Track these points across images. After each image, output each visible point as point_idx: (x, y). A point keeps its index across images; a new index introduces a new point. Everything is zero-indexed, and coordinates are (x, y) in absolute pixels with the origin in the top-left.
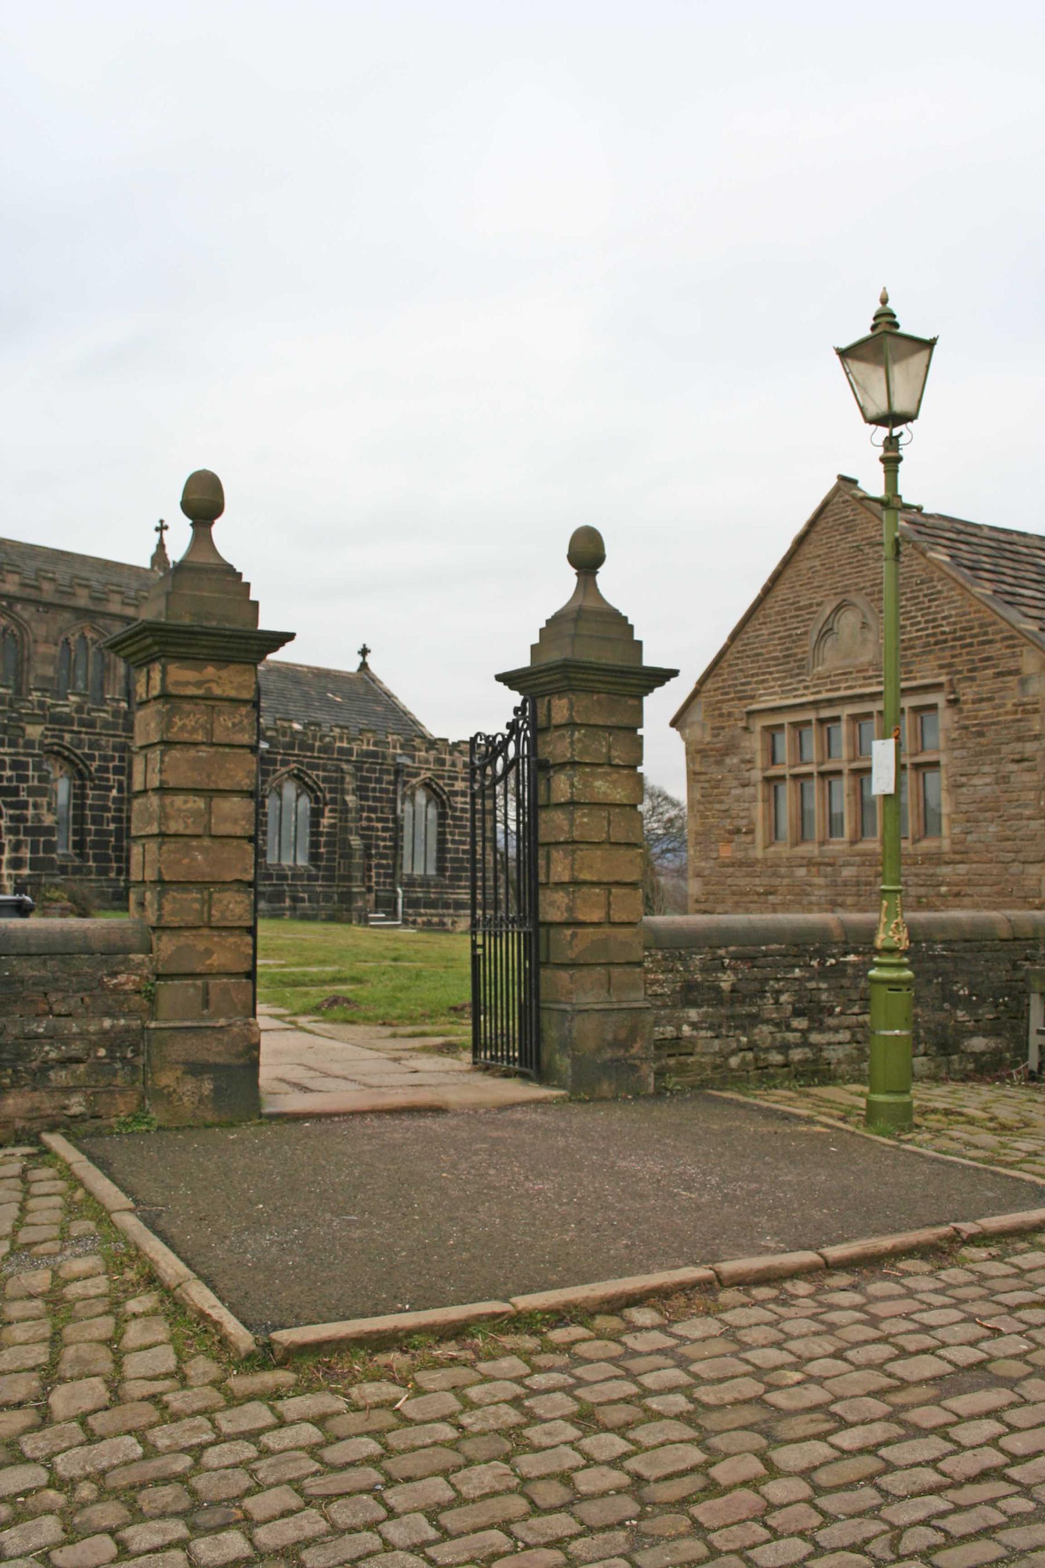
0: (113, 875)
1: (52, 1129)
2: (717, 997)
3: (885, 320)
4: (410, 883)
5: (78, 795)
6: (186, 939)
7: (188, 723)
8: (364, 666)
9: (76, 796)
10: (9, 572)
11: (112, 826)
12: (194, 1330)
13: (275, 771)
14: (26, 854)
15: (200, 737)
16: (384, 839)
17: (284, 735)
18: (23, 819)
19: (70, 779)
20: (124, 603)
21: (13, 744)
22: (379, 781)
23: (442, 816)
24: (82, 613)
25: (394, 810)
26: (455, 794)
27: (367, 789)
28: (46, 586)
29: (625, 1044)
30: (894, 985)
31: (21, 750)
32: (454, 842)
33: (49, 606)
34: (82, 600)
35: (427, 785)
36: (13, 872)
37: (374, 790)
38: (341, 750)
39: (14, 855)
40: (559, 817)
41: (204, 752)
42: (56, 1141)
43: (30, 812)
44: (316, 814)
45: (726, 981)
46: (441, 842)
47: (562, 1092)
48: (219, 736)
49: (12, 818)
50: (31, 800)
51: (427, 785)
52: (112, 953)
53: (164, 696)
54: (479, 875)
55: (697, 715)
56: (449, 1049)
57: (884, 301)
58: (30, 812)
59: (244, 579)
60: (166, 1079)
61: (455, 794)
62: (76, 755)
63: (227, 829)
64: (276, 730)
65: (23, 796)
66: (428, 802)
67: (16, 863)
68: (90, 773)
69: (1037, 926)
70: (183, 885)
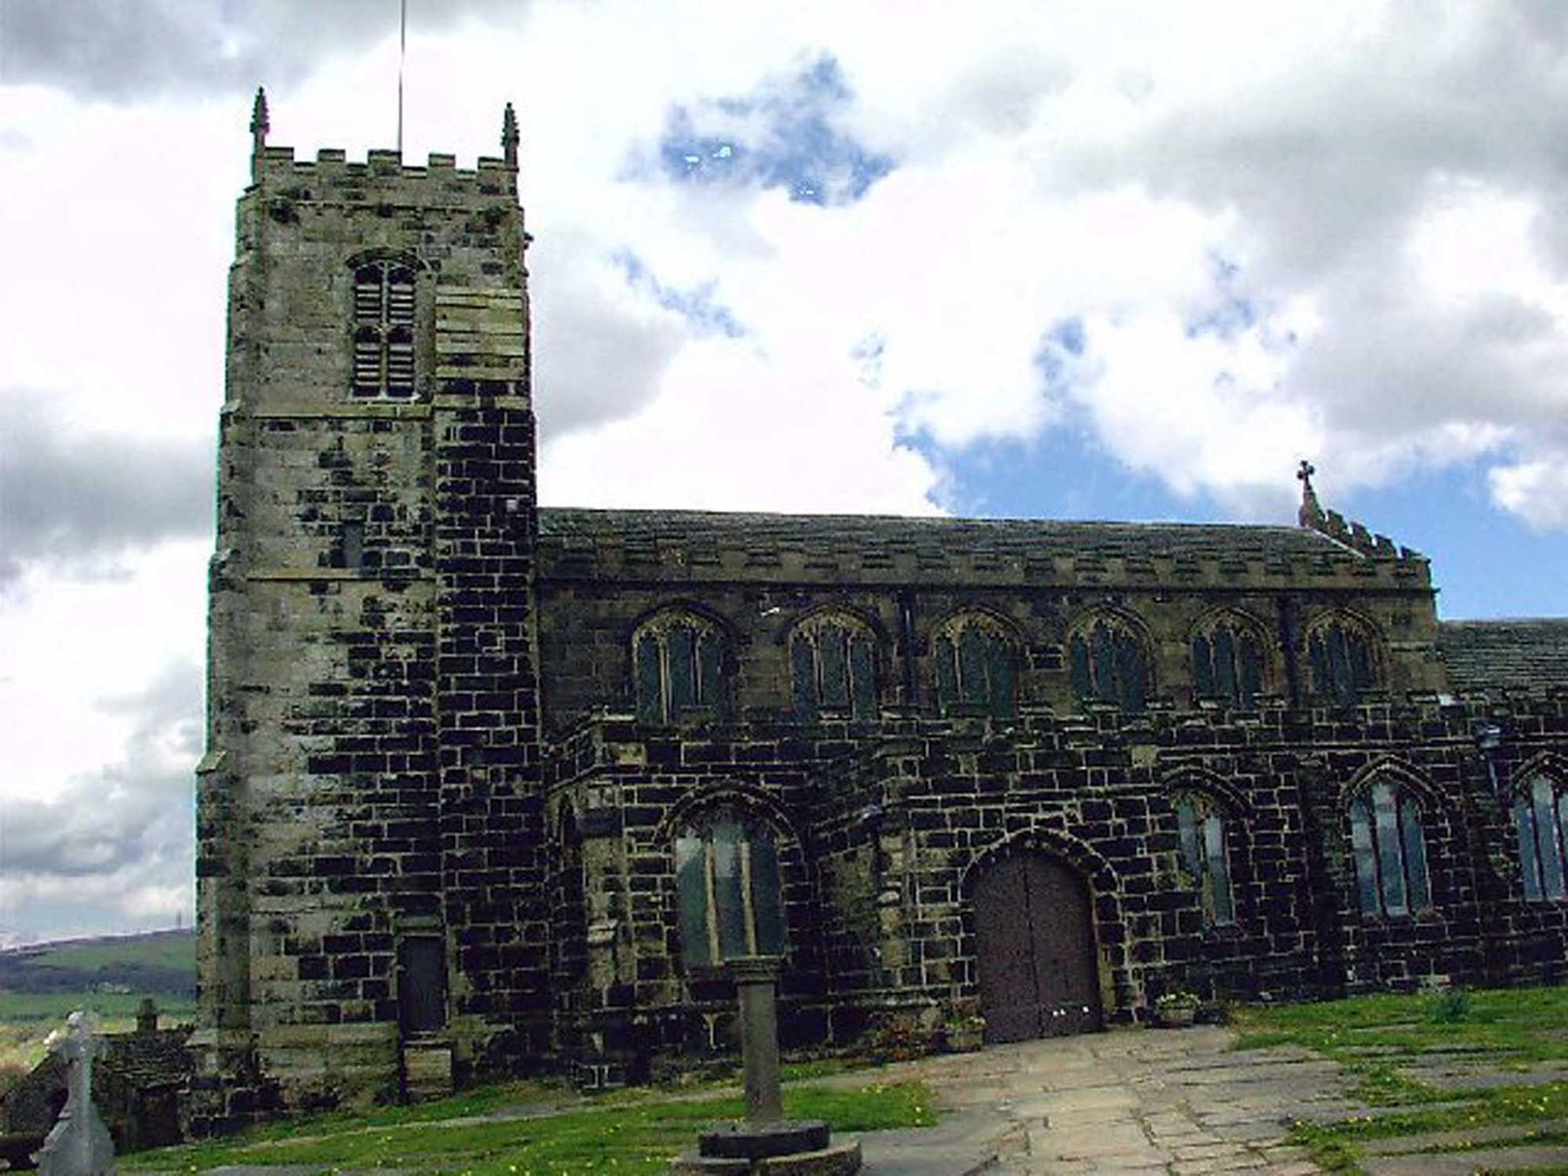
0: (1300, 947)
5: (1234, 839)
9: (1232, 842)
10: (1109, 556)
11: (1290, 878)
13: (1516, 766)
14: (1155, 936)
17: (1521, 711)
18: (1147, 885)
19: (1223, 818)
20: (1268, 572)
21: (1115, 777)
24: (1213, 595)
28: (1161, 567)
31: (1130, 786)
33: (1167, 593)
34: (1212, 576)
36: (1140, 965)
39: (1138, 940)
43: (1155, 875)
50: (1153, 856)
54: (1209, 782)
58: (1155, 875)
59: (415, 157)
62: (1224, 784)
64: (1508, 706)
67: (1144, 952)
68: (1246, 804)
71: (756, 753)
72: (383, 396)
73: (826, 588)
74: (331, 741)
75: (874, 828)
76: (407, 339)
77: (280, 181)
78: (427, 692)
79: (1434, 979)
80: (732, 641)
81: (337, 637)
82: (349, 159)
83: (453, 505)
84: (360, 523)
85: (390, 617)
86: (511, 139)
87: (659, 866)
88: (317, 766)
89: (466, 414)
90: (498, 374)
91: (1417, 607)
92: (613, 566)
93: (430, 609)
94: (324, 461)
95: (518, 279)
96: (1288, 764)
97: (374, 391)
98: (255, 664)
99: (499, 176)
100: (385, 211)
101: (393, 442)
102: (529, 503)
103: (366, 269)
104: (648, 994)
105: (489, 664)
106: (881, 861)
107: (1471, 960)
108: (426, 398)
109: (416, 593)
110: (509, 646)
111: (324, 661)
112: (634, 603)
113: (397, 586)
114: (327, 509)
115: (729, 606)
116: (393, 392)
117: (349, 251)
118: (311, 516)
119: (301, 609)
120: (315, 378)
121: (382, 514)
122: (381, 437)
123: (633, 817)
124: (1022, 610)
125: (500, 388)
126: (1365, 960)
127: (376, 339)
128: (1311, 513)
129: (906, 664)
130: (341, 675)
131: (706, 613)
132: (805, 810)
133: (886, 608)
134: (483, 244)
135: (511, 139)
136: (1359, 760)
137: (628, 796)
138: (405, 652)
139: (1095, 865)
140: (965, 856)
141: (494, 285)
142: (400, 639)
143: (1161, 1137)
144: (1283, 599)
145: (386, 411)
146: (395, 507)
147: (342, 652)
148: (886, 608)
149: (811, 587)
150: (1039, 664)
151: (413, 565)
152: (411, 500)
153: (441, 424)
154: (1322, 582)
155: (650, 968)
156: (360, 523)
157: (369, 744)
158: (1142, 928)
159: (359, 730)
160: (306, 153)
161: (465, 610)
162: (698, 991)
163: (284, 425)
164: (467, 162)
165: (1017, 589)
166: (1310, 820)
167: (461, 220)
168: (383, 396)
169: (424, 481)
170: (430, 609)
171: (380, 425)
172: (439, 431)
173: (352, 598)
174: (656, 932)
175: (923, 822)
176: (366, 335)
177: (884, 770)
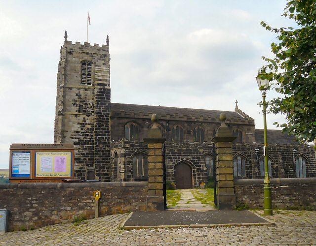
2: (251, 194)
6: (152, 184)
14: (201, 176)
16: (291, 169)
22: (288, 156)
23: (307, 163)
26: (310, 158)
27: (285, 158)
28: (209, 119)
29: (230, 201)
32: (310, 169)
35: (302, 156)
37: (287, 158)
38: (278, 149)
41: (154, 157)
44: (273, 164)
45: (253, 191)
46: (307, 169)
49: (198, 169)
52: (142, 186)
59: (92, 44)
61: (310, 158)
65: (200, 164)
66: (302, 160)
69: (315, 180)
74: (77, 140)
81: (79, 123)
85: (87, 121)
86: (108, 41)
87: (131, 162)
89: (100, 89)
90: (105, 83)
91: (251, 127)
94: (77, 95)
97: (85, 84)
99: (105, 48)
101: (88, 92)
103: (83, 63)
105: (103, 129)
108: (93, 86)
110: (106, 126)
111: (77, 127)
112: (125, 121)
113: (89, 116)
114: (77, 103)
115: (140, 122)
117: (81, 60)
118: (75, 104)
119: (73, 119)
120: (75, 80)
121: (86, 104)
130: (79, 130)
131: (134, 122)
134: (103, 60)
135: (108, 41)
136: (236, 153)
138: (89, 127)
139: (193, 165)
140: (174, 163)
141: (104, 67)
142: (89, 124)
145: (87, 88)
146: (88, 103)
147: (79, 126)
151: (91, 112)
152: (91, 102)
153: (96, 91)
154: (235, 123)
157: (83, 140)
158: (199, 175)
159: (82, 138)
161: (99, 121)
163: (71, 89)
164: (100, 45)
165: (185, 121)
169: (93, 99)
171: (86, 90)
174: (130, 171)
175: (169, 158)
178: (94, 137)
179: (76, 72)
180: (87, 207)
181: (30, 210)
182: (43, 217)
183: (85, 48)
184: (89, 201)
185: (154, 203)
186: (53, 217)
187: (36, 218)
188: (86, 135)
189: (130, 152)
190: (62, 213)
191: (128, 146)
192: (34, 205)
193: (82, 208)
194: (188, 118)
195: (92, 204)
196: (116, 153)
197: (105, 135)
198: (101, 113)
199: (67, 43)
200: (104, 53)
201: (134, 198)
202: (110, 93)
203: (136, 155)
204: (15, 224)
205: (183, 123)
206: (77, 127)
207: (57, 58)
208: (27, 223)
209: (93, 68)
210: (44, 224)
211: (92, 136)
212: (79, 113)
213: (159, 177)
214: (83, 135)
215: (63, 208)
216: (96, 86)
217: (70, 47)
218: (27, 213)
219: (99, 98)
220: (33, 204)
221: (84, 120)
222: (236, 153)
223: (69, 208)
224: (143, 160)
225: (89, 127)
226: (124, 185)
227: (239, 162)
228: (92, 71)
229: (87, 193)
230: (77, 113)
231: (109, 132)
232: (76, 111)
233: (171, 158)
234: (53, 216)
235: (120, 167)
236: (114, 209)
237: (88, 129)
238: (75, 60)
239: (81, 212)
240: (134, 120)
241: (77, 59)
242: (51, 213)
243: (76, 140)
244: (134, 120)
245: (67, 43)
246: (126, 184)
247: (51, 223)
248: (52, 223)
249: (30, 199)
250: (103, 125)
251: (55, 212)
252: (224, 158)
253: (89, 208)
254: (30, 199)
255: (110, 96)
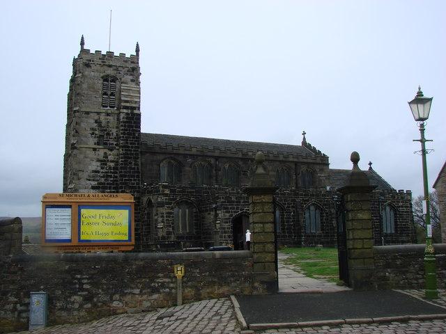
1: (233, 294)
3: (420, 94)
4: (386, 235)
6: (259, 254)
7: (258, 208)
8: (371, 168)
12: (238, 323)
15: (261, 211)
23: (395, 214)
25: (379, 213)
28: (270, 155)
30: (430, 262)
34: (281, 158)
35: (389, 205)
40: (350, 223)
42: (233, 298)
46: (396, 222)
47: (347, 289)
48: (265, 210)
51: (389, 205)
52: (244, 258)
53: (253, 203)
55: (439, 184)
56: (333, 280)
57: (420, 89)
59: (117, 54)
60: (256, 284)
63: (268, 230)
70: (259, 243)
71: (190, 192)
72: (108, 108)
73: (200, 156)
74: (96, 183)
75: (216, 209)
76: (114, 96)
77: (86, 57)
78: (117, 173)
79: (319, 245)
80: (180, 166)
81: (98, 160)
82: (102, 53)
83: (124, 134)
84: (103, 136)
85: (109, 157)
86: (137, 50)
88: (93, 188)
89: (127, 114)
90: (134, 105)
91: (325, 167)
92: (157, 150)
93: (118, 155)
94: (96, 122)
95: (138, 83)
96: (295, 200)
97: (107, 107)
98: (82, 166)
99: (135, 60)
100: (110, 66)
101: (110, 118)
102: (140, 133)
103: (105, 79)
104: (168, 238)
105: (131, 168)
106: (216, 215)
107: (328, 242)
108: (118, 109)
109: (115, 152)
110: (135, 164)
111: (95, 166)
112: (161, 157)
113: (111, 150)
114: (97, 132)
115: (180, 159)
116: (110, 107)
117: (102, 75)
118: (93, 134)
119: (91, 154)
120: (94, 103)
121: (108, 134)
122: (108, 117)
123: (167, 203)
124: (240, 163)
125: (135, 108)
126: (305, 241)
127: (107, 95)
128: (304, 142)
129: (216, 173)
130: (99, 169)
131: (174, 159)
132: (199, 205)
133: (213, 161)
134: (131, 75)
135: (137, 50)
136: (308, 201)
137: (166, 199)
138: (112, 165)
141: (133, 85)
142: (112, 162)
143: (223, 303)
144: (296, 164)
145: (109, 112)
147: (99, 164)
148: (213, 161)
149: (197, 155)
150: (244, 174)
152: (114, 131)
153: (122, 116)
154: (305, 160)
155: (169, 233)
156: (103, 136)
160: (93, 51)
161: (126, 156)
162: (178, 238)
163: (87, 113)
164: (128, 56)
165: (240, 158)
166: (297, 211)
167: (127, 69)
168: (108, 108)
169: (117, 128)
170: (118, 155)
171: (108, 115)
172: (121, 117)
173: (101, 153)
176: (105, 94)
177: (218, 198)
178: (119, 178)
179: (96, 91)
180: (165, 288)
181: (79, 293)
182: (100, 304)
183: (107, 59)
184: (167, 280)
185: (262, 282)
186: (115, 304)
187: (89, 305)
188: (108, 176)
189: (170, 199)
190: (128, 298)
191: (167, 191)
192: (85, 286)
193: (155, 290)
194: (243, 154)
195: (172, 285)
196: (150, 201)
197: (133, 176)
198: (128, 147)
199: (84, 51)
200: (133, 65)
201: (233, 276)
202: (139, 119)
203: (179, 204)
204: (58, 313)
205: (237, 160)
206: (95, 166)
207: (69, 72)
208: (75, 313)
209: (118, 86)
210: (99, 316)
211: (116, 177)
212: (98, 147)
213: (269, 245)
214: (103, 177)
215: (129, 291)
216: (121, 110)
217: (88, 57)
218: (75, 297)
219: (125, 126)
220: (84, 284)
221: (106, 156)
222: (308, 201)
223: (137, 291)
224: (187, 210)
225: (112, 165)
226: (217, 257)
227: (312, 213)
228: (117, 90)
229: (164, 269)
230: (95, 146)
231: (138, 172)
232: (95, 144)
233: (227, 208)
234: (115, 302)
235: (156, 220)
236: (204, 292)
237: (110, 168)
238: (94, 74)
239: (155, 296)
240: (172, 156)
241: (97, 74)
242: (111, 298)
243: (94, 183)
244: (172, 156)
245: (84, 51)
246: (222, 255)
247: (111, 313)
248: (114, 313)
249: (79, 276)
250: (131, 163)
251: (117, 296)
252: (360, 216)
253: (167, 290)
254: (79, 276)
255: (139, 123)
